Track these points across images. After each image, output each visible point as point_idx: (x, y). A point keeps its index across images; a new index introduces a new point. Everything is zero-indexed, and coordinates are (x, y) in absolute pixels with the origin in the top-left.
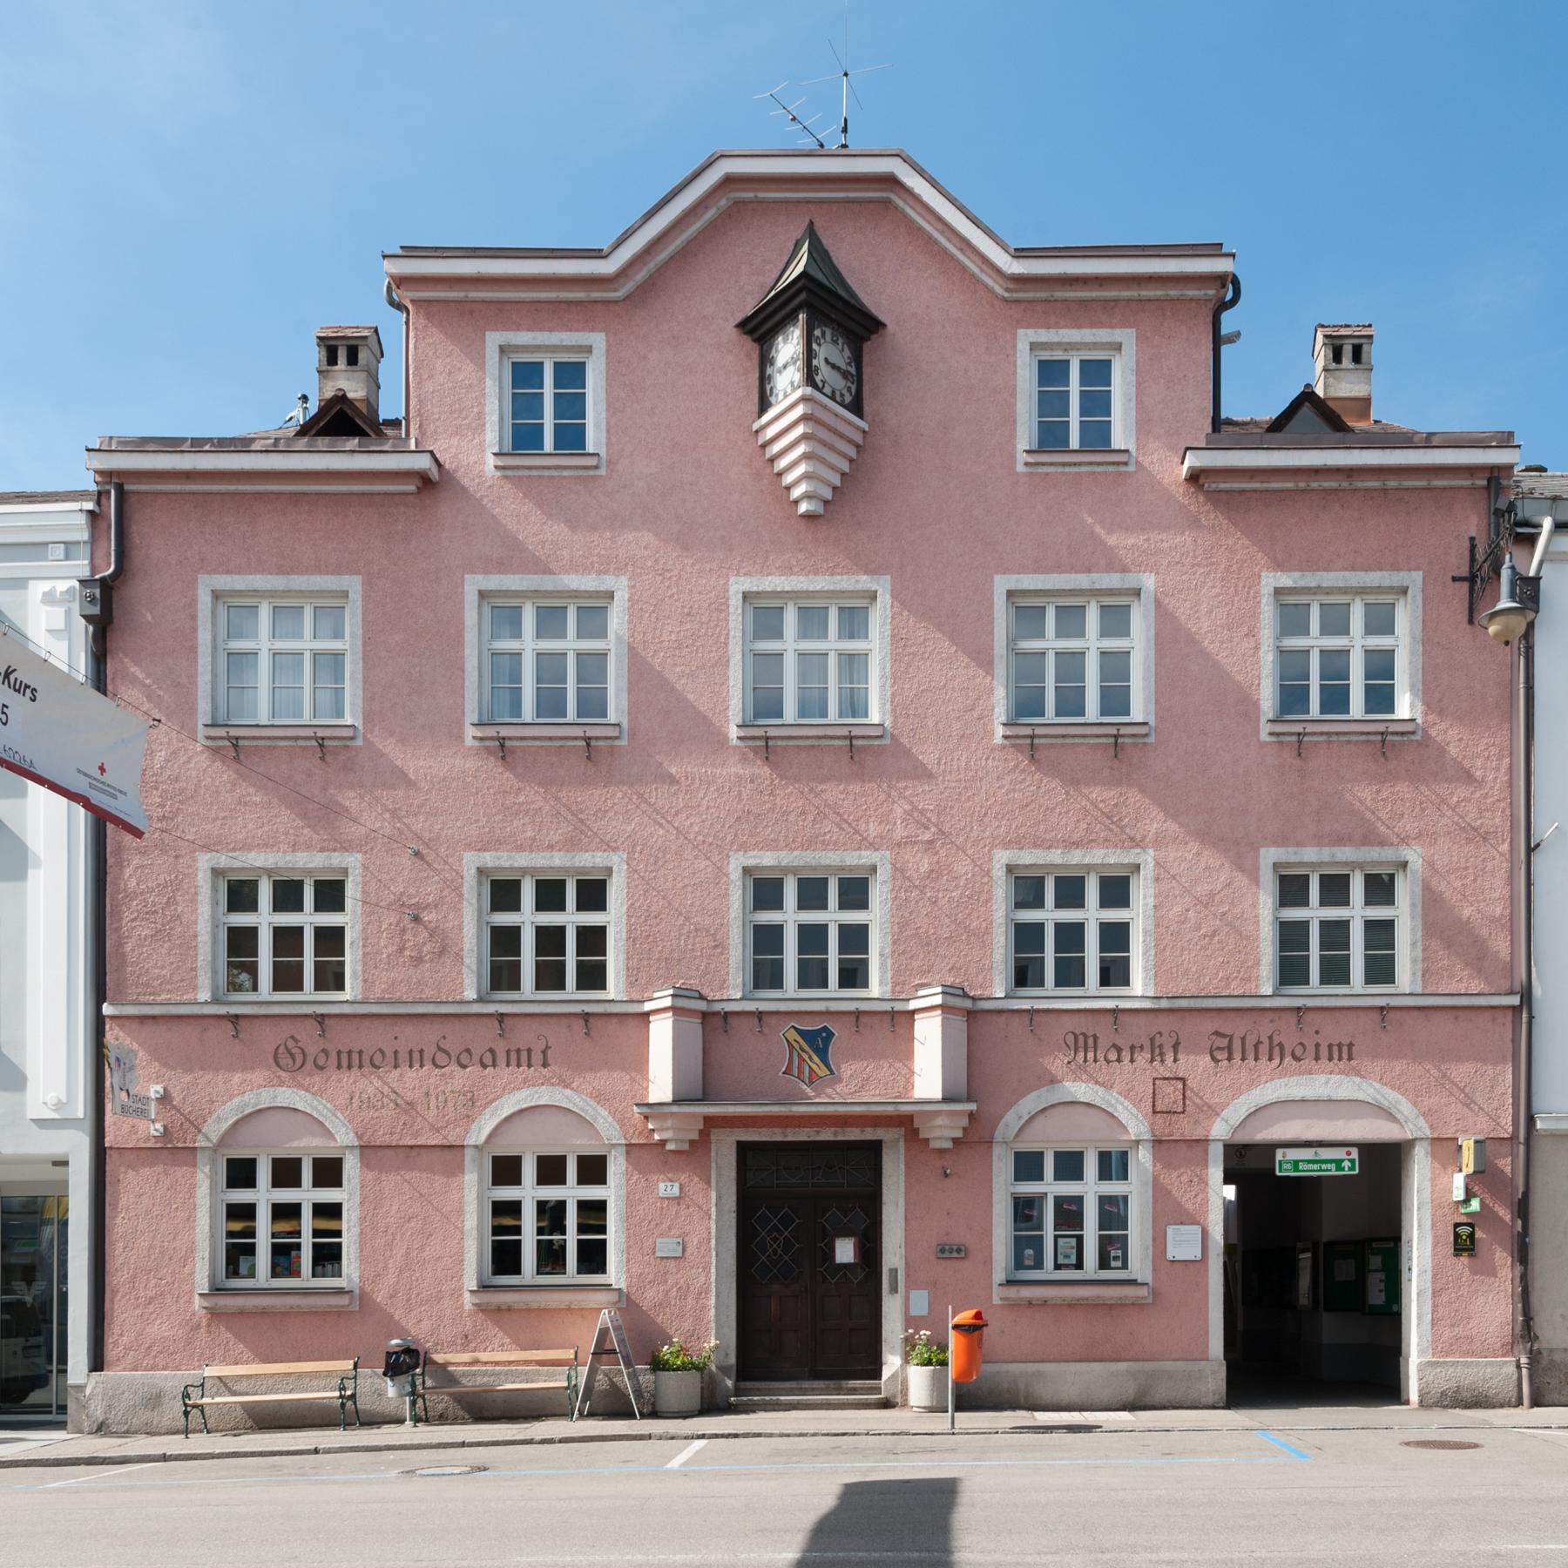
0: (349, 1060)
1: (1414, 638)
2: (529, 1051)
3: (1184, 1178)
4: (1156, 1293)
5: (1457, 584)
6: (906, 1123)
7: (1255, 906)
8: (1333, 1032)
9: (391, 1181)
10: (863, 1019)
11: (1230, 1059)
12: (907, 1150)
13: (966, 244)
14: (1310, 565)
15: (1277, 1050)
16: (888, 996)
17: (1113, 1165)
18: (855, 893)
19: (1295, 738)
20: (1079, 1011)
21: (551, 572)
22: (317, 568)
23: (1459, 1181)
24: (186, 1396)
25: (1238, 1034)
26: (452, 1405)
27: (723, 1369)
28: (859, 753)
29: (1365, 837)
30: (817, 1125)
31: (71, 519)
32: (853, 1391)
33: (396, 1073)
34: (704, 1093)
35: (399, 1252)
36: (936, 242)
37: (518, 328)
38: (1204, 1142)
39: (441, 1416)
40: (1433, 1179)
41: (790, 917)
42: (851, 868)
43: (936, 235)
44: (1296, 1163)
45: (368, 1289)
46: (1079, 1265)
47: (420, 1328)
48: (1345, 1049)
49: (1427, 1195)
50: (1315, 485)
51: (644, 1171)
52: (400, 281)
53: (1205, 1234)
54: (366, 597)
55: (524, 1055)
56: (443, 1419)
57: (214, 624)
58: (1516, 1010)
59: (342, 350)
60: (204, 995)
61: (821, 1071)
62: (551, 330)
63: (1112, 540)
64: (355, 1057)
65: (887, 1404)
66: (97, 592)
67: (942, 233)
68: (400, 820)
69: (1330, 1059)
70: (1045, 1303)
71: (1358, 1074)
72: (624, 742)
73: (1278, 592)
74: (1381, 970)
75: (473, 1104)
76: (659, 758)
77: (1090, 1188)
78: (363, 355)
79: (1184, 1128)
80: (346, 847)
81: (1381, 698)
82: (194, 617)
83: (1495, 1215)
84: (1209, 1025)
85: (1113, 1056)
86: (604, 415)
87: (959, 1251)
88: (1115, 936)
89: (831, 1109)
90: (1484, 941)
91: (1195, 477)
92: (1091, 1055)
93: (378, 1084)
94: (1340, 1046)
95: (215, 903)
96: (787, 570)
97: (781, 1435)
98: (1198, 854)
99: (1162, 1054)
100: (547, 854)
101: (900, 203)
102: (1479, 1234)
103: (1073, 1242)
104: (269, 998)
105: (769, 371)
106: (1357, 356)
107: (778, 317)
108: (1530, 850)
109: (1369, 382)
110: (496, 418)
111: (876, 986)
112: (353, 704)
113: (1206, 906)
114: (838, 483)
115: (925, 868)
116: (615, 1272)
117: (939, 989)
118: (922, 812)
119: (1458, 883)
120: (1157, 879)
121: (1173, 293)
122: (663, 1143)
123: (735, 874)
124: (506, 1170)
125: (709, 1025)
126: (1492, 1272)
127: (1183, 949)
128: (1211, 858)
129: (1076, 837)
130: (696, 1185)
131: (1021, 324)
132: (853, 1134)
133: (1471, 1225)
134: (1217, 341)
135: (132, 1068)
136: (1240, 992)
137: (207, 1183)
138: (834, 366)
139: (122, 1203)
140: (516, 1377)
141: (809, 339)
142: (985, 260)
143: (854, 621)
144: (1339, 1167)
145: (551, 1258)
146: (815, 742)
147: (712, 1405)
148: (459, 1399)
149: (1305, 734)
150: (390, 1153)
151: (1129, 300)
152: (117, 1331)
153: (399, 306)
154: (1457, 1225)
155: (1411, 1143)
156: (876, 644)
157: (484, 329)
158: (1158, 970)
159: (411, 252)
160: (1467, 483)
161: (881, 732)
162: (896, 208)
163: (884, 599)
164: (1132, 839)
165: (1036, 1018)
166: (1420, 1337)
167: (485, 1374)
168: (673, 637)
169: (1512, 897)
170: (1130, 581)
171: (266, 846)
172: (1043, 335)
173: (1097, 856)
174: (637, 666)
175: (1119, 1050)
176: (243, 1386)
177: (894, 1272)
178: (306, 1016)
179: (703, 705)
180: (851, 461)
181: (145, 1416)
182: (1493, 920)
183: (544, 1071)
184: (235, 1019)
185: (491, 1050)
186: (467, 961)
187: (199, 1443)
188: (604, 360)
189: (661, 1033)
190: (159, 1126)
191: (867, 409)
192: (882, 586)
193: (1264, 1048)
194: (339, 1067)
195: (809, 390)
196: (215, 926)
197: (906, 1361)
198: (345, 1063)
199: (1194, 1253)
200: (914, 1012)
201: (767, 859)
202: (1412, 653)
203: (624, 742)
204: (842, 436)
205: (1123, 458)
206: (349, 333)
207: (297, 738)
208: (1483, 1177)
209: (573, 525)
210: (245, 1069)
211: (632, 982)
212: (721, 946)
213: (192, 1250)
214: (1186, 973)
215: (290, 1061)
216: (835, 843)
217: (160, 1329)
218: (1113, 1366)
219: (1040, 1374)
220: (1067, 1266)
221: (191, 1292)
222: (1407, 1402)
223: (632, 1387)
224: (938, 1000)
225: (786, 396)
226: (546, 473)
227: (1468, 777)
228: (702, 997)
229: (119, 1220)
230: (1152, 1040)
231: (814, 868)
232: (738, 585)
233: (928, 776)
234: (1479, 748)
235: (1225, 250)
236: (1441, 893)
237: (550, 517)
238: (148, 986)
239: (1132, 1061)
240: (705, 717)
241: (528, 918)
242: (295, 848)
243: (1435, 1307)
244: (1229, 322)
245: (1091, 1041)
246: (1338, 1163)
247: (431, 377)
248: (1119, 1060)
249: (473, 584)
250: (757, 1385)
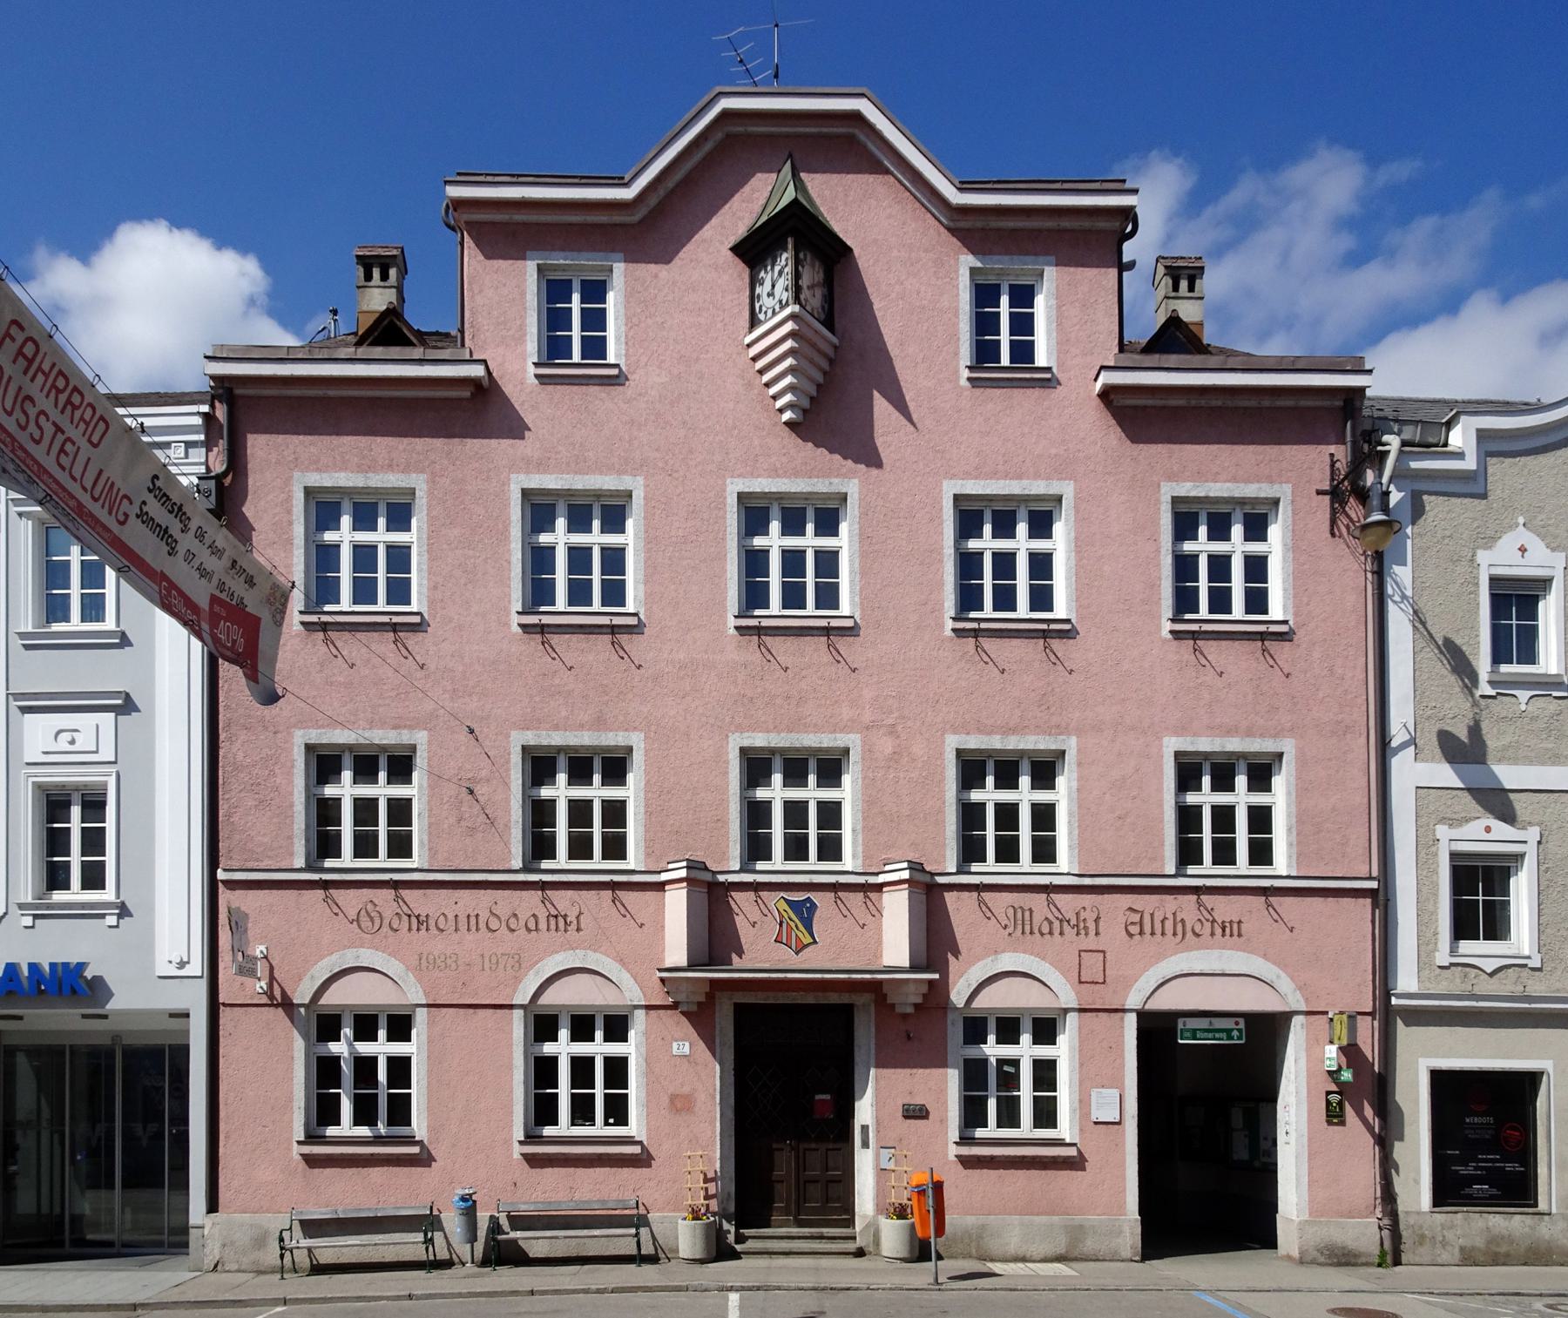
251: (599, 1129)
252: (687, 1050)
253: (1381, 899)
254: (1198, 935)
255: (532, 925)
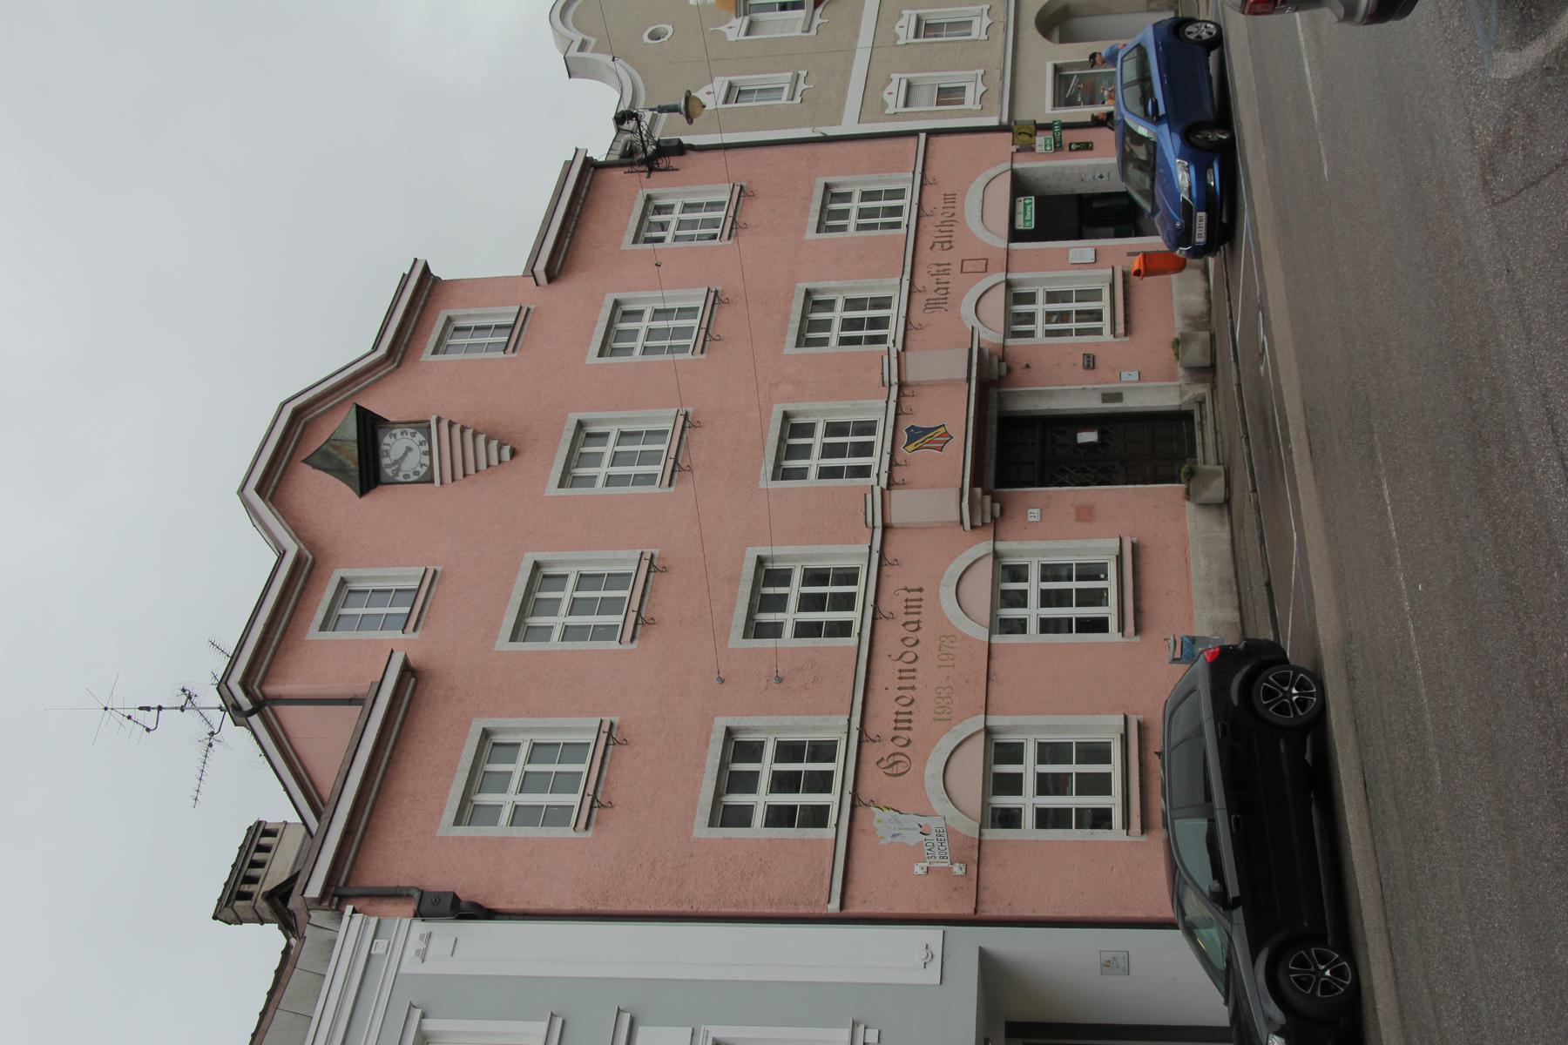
82: (474, 839)
97: (1262, 542)
251: (1114, 768)
252: (1036, 511)
253: (931, 133)
254: (909, 742)
255: (914, 626)
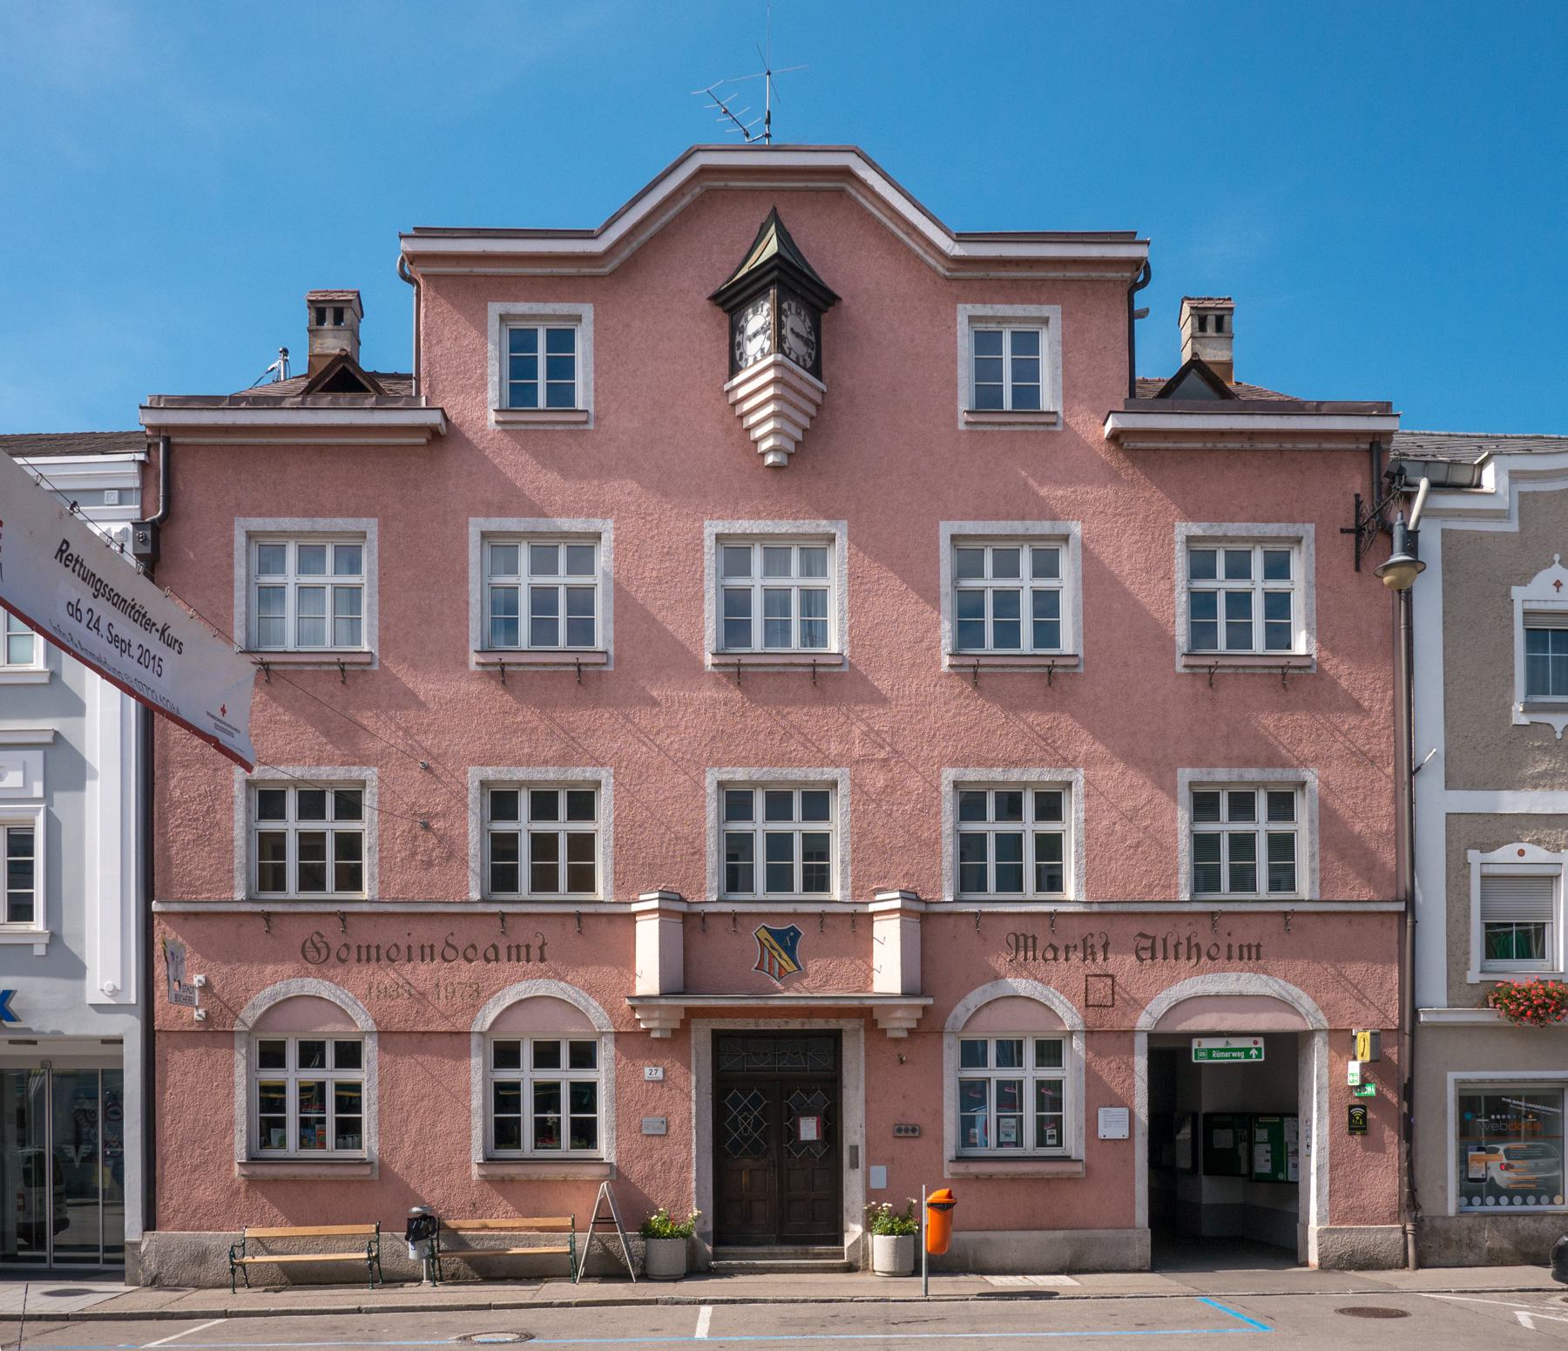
0: (369, 954)
1: (1308, 582)
2: (528, 947)
3: (1113, 1065)
4: (1088, 1169)
5: (1345, 536)
6: (867, 1015)
7: (1174, 820)
8: (1245, 934)
9: (405, 1064)
10: (828, 920)
11: (1153, 958)
12: (866, 1039)
13: (912, 229)
14: (1217, 517)
15: (1194, 950)
16: (849, 899)
17: (1050, 1052)
18: (817, 804)
19: (1206, 670)
20: (1020, 914)
21: (544, 515)
22: (339, 512)
23: (1354, 1068)
24: (232, 1256)
25: (1161, 936)
26: (463, 1266)
27: (702, 1235)
28: (822, 680)
29: (1269, 759)
30: (786, 1016)
31: (123, 466)
32: (818, 1256)
33: (409, 967)
34: (685, 986)
35: (414, 1128)
36: (884, 227)
37: (516, 299)
38: (1131, 1033)
39: (453, 1275)
40: (1330, 1067)
41: (759, 826)
42: (814, 783)
43: (885, 220)
44: (1210, 1051)
45: (387, 1160)
46: (1018, 1143)
47: (433, 1195)
48: (1254, 950)
49: (1325, 1080)
50: (1220, 446)
51: (631, 1057)
52: (414, 258)
53: (1132, 1115)
54: (382, 537)
55: (523, 950)
56: (455, 1279)
57: (248, 563)
58: (1402, 915)
59: (331, 311)
60: (240, 895)
61: (790, 967)
62: (545, 301)
63: (1044, 492)
64: (373, 951)
65: (850, 1268)
66: (149, 533)
67: (890, 219)
68: (412, 737)
69: (1241, 958)
70: (990, 1177)
71: (1265, 972)
72: (611, 668)
73: (1190, 539)
74: (1283, 878)
75: (478, 995)
76: (642, 683)
77: (1029, 1073)
78: (348, 316)
79: (1113, 1020)
80: (365, 762)
81: (1279, 635)
82: (230, 555)
83: (1384, 1097)
84: (1134, 927)
85: (1050, 955)
86: (592, 376)
87: (914, 1130)
88: (1050, 847)
89: (802, 1003)
90: (1374, 853)
91: (1115, 437)
92: (1030, 954)
93: (393, 975)
94: (1249, 947)
95: (248, 811)
96: (756, 515)
98: (1123, 773)
99: (1093, 954)
100: (543, 769)
101: (853, 192)
102: (1370, 1115)
103: (1013, 1122)
104: (296, 897)
105: (738, 338)
106: (1220, 325)
107: (749, 291)
108: (1412, 773)
109: (1231, 349)
110: (496, 379)
111: (837, 891)
112: (369, 632)
113: (1131, 820)
114: (800, 438)
115: (881, 784)
116: (605, 1147)
117: (657, 895)
118: (878, 733)
119: (1350, 802)
120: (1087, 796)
121: (1094, 275)
122: (648, 1031)
123: (711, 788)
124: (506, 1055)
125: (688, 926)
126: (1381, 1149)
127: (1110, 859)
128: (1134, 777)
129: (1014, 757)
130: (677, 1069)
131: (959, 299)
132: (818, 1024)
133: (1363, 1107)
134: (1132, 316)
135: (182, 960)
136: (1161, 898)
137: (244, 1063)
138: (798, 335)
139: (170, 1080)
140: (518, 1241)
141: (779, 313)
142: (929, 243)
143: (814, 564)
144: (1248, 1056)
145: (546, 1133)
146: (782, 669)
147: (696, 1269)
148: (469, 1261)
149: (1217, 667)
150: (403, 1038)
151: (1055, 280)
152: (167, 1195)
153: (410, 280)
154: (1351, 1107)
155: (1310, 1034)
156: (834, 582)
157: (486, 300)
158: (1089, 877)
159: (422, 233)
160: (1353, 446)
161: (840, 660)
162: (849, 196)
163: (842, 541)
164: (1065, 759)
165: (983, 920)
166: (1319, 1207)
167: (492, 1238)
168: (654, 574)
169: (1397, 817)
170: (1060, 528)
171: (293, 760)
172: (981, 310)
173: (1033, 774)
174: (623, 602)
175: (1055, 950)
176: (278, 1246)
177: (854, 1149)
178: (329, 914)
179: (681, 635)
180: (812, 418)
181: (193, 1271)
182: (1381, 835)
183: (542, 966)
184: (268, 916)
185: (494, 946)
186: (472, 865)
187: (248, 1299)
188: (591, 328)
189: (648, 934)
190: (201, 1011)
191: (825, 372)
192: (840, 529)
193: (1183, 949)
194: (359, 960)
195: (780, 357)
196: (249, 832)
197: (868, 1228)
198: (364, 956)
199: (1121, 1132)
200: (872, 914)
201: (740, 774)
202: (1307, 596)
203: (611, 668)
204: (804, 396)
205: (1052, 419)
206: (336, 297)
207: (320, 664)
208: (1376, 1067)
209: (565, 473)
210: (276, 961)
211: (619, 885)
212: (699, 853)
213: (231, 1123)
214: (1114, 879)
215: (316, 955)
216: (801, 760)
217: (205, 1193)
218: (1050, 1234)
219: (987, 1241)
220: (1008, 1144)
221: (231, 1161)
222: (1306, 1264)
223: (629, 1252)
224: (655, 904)
225: (756, 361)
226: (541, 427)
227: (1357, 707)
228: (682, 899)
229: (167, 1096)
230: (1084, 941)
231: (780, 783)
232: (712, 528)
233: (883, 701)
234: (1365, 682)
235: (1137, 238)
236: (1335, 811)
237: (544, 466)
238: (191, 885)
239: (1067, 959)
240: (683, 646)
241: (524, 826)
242: (318, 762)
243: (1332, 1180)
244: (1141, 299)
245: (1030, 941)
246: (1247, 1051)
247: (439, 342)
248: (1055, 959)
249: (476, 526)
250: (732, 1249)
